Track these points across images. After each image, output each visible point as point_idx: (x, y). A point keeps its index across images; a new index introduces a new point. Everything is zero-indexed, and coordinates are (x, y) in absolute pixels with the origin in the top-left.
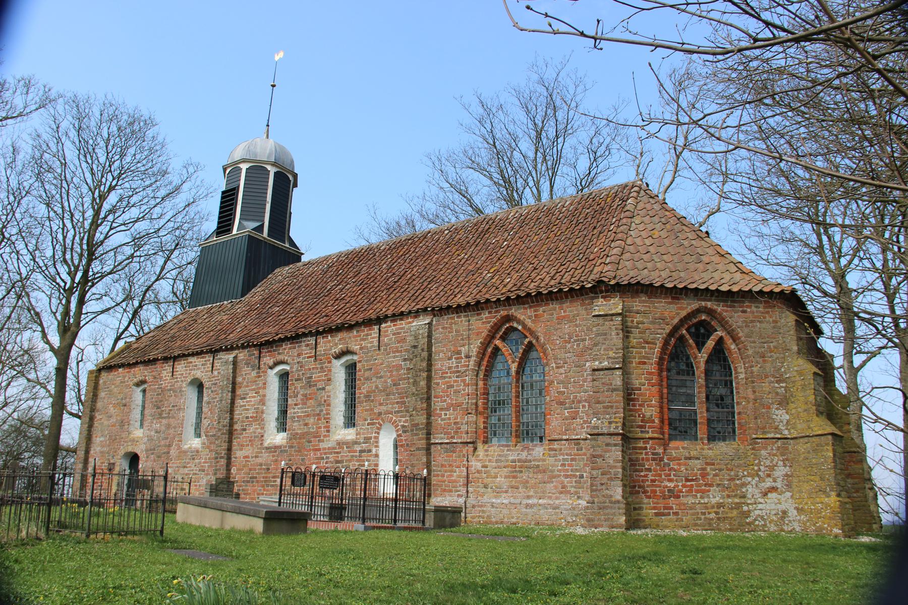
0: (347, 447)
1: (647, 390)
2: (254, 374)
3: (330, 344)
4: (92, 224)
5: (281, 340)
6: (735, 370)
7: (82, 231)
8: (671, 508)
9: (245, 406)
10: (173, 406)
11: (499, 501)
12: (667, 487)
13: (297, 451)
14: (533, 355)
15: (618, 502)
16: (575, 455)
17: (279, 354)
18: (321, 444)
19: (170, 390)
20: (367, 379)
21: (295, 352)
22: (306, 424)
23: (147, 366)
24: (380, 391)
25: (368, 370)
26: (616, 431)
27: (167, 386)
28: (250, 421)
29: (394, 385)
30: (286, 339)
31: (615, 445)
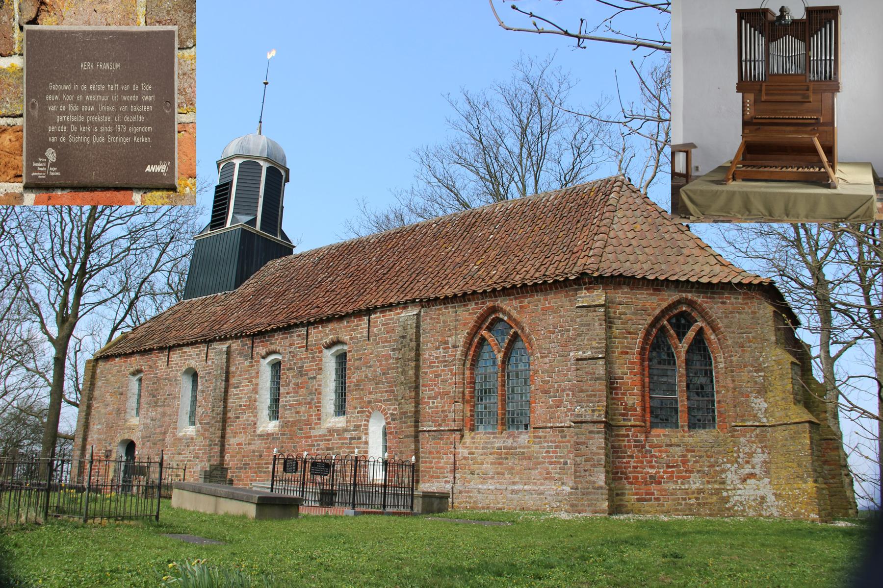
0: (337, 435)
1: (629, 379)
2: (247, 363)
3: (321, 335)
4: (89, 218)
5: (273, 331)
6: (715, 360)
7: (79, 225)
8: (653, 494)
9: (238, 394)
10: (168, 395)
11: (485, 487)
12: (648, 473)
13: (288, 438)
14: (519, 345)
15: (601, 488)
16: (559, 442)
17: (271, 344)
18: (312, 431)
19: (166, 379)
20: (357, 368)
21: (287, 342)
22: (298, 413)
23: (143, 355)
24: (370, 380)
25: (358, 359)
26: (599, 419)
27: (162, 375)
28: (243, 409)
29: (384, 374)
30: (279, 329)
31: (598, 433)
